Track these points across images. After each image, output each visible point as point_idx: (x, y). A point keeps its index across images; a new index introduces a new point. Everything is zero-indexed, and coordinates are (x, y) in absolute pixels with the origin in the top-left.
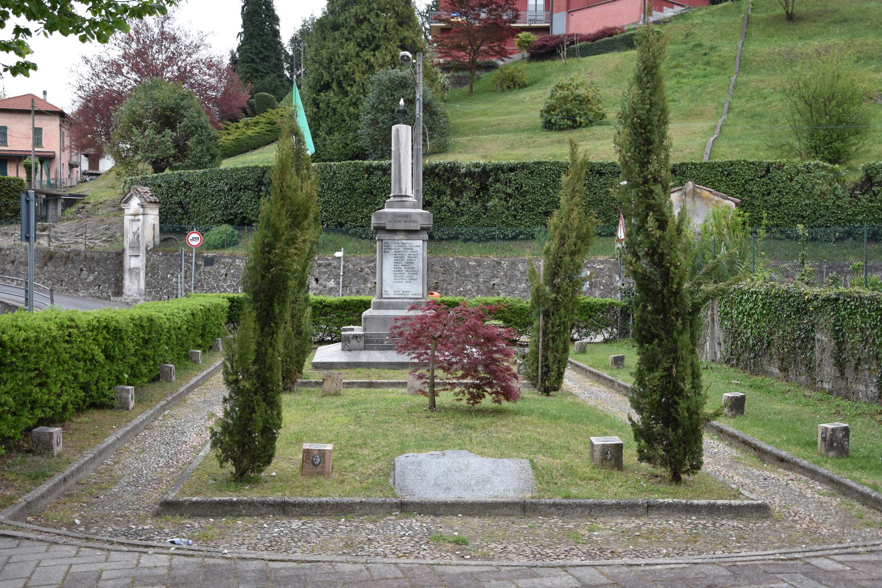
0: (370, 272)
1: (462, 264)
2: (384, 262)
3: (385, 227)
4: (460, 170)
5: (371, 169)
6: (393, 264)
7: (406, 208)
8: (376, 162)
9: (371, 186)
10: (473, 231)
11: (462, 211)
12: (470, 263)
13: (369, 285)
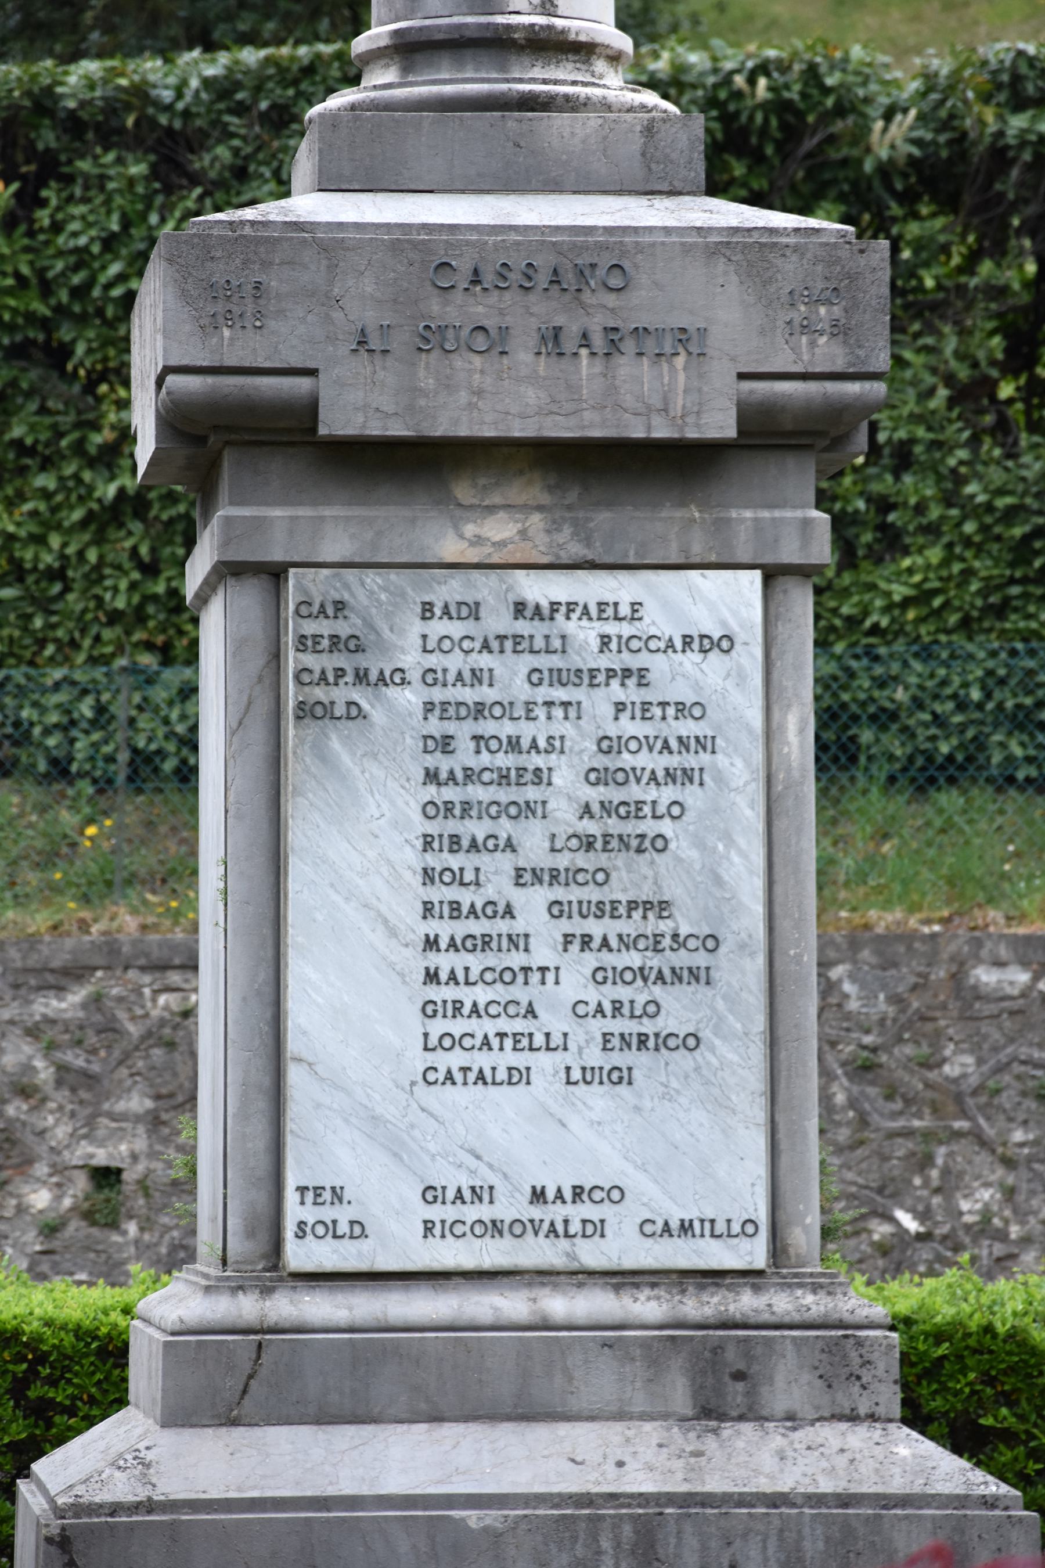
0: (44, 1072)
1: (905, 977)
2: (296, 835)
3: (311, 409)
4: (860, 136)
5: (48, 138)
6: (412, 858)
7: (553, 186)
8: (91, 67)
9: (46, 289)
10: (991, 682)
11: (884, 505)
12: (985, 976)
13: (40, 1199)
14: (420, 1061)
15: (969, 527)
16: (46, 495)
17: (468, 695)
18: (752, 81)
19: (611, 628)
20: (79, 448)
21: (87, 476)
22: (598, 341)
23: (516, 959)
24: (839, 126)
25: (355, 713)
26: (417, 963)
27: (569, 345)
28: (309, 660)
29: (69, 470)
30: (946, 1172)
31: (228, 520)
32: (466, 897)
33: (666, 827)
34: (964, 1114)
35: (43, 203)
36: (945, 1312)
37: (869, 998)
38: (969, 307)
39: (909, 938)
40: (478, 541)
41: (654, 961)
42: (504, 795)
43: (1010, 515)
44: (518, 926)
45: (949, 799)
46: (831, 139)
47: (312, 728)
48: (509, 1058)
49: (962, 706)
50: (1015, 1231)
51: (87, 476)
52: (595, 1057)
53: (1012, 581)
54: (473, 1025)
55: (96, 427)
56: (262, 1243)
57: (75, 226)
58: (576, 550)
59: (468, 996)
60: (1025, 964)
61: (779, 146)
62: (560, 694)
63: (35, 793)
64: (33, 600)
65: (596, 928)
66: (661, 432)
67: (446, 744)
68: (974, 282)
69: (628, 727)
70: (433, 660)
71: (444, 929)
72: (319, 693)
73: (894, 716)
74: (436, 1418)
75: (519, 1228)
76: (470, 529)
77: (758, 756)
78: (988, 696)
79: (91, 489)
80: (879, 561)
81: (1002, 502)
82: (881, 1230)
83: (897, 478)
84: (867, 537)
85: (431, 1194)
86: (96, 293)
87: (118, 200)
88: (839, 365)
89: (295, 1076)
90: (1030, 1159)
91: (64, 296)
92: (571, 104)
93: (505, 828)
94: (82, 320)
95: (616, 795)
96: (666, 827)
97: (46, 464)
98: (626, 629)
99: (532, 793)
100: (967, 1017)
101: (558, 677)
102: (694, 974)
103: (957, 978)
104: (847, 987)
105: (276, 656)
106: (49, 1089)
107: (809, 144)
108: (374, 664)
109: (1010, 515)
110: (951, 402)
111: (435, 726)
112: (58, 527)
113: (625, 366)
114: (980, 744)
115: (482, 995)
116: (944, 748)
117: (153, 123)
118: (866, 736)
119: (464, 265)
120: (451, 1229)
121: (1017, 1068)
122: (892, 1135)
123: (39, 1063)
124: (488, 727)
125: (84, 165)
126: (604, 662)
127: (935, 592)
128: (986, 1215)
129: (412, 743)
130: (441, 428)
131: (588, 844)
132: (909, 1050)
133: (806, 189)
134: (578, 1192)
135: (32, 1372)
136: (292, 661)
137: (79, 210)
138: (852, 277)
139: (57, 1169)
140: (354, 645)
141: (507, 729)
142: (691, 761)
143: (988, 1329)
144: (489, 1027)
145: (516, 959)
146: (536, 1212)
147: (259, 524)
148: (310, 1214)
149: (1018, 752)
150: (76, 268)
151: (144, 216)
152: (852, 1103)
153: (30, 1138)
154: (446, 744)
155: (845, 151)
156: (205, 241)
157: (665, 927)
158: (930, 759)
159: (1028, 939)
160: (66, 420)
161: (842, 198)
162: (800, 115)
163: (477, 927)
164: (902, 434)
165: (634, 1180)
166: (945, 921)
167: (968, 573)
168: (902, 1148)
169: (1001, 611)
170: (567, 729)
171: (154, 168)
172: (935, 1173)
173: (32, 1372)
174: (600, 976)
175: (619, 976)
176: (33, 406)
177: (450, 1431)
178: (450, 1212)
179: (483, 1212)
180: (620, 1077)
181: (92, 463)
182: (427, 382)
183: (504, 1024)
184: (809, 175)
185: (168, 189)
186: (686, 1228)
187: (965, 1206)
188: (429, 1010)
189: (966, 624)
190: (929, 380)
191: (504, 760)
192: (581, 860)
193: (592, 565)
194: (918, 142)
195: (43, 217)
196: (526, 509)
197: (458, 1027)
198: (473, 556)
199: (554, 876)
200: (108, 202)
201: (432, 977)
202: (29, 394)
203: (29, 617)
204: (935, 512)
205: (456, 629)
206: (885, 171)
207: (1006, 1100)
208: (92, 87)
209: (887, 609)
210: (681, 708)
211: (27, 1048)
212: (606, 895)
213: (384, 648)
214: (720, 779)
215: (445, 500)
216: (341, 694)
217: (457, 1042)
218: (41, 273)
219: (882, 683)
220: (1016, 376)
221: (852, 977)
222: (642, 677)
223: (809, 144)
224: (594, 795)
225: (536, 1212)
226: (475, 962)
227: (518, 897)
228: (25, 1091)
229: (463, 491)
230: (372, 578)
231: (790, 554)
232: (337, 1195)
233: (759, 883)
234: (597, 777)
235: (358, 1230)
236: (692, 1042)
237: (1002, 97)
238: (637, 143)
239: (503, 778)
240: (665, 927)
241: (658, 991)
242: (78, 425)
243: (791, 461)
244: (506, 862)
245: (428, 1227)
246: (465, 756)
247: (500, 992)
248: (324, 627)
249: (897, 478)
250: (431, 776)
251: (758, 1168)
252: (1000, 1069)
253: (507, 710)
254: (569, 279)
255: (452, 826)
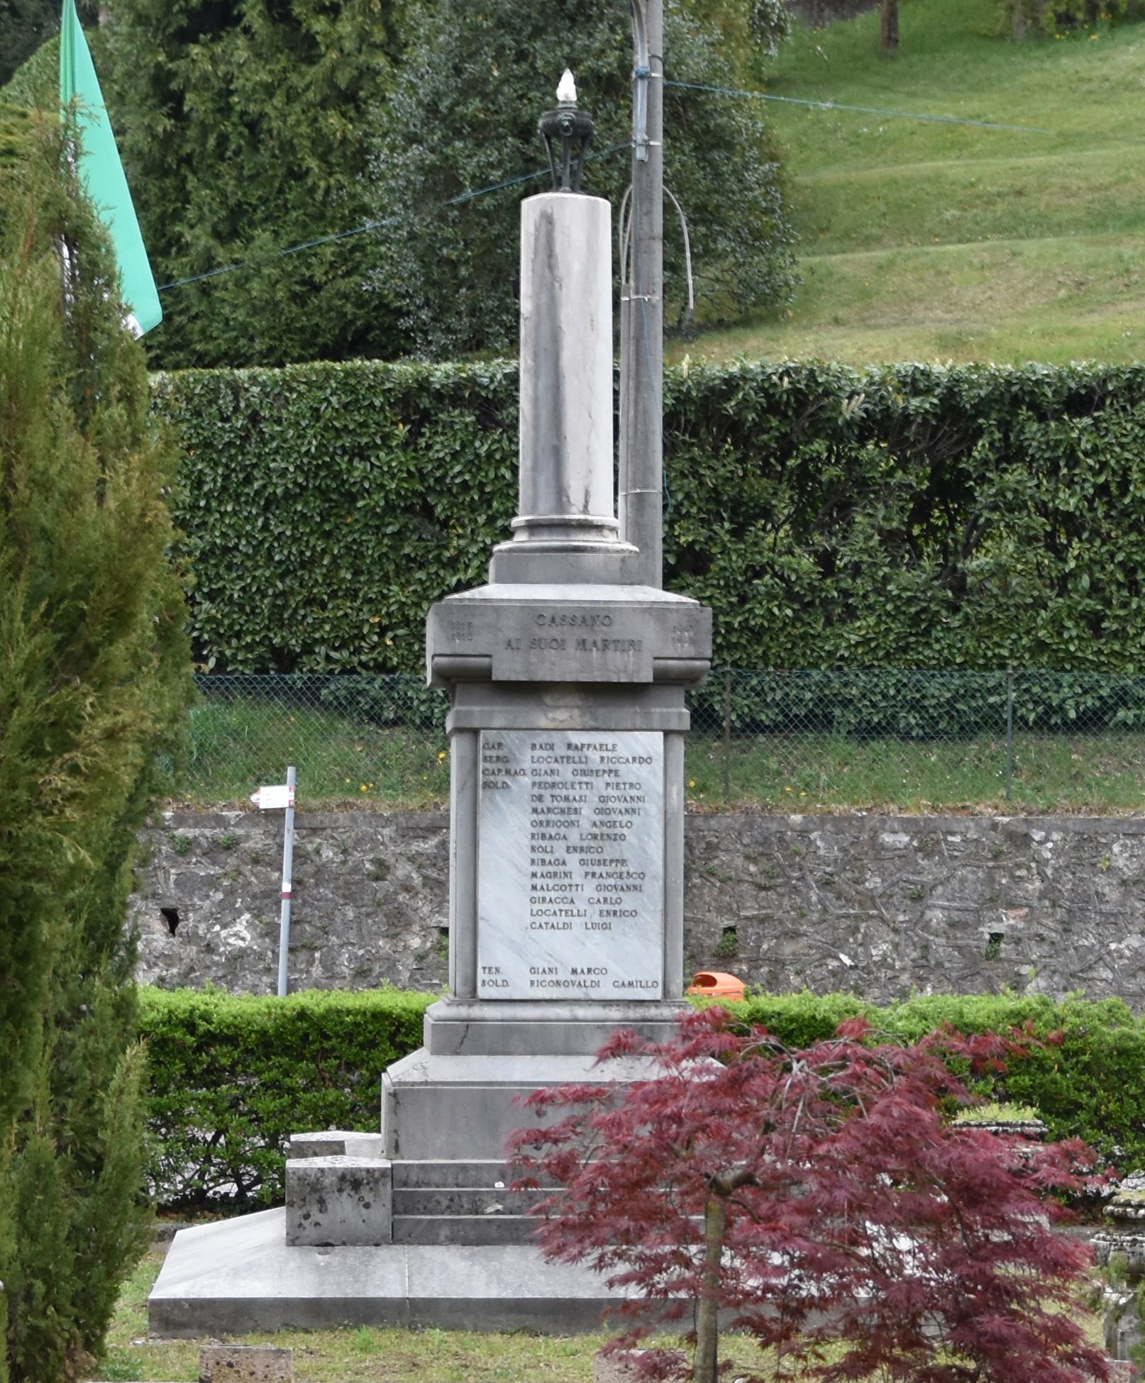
0: (417, 880)
1: (847, 839)
2: (483, 832)
5: (425, 402)
6: (527, 842)
8: (447, 366)
9: (423, 477)
11: (846, 593)
12: (887, 838)
13: (415, 942)
14: (529, 920)
15: (889, 607)
16: (421, 582)
17: (549, 779)
18: (781, 379)
19: (605, 754)
20: (438, 559)
21: (442, 573)
22: (600, 644)
23: (566, 881)
24: (826, 401)
25: (505, 786)
26: (528, 882)
27: (588, 646)
28: (488, 765)
29: (433, 569)
30: (865, 935)
31: (458, 712)
32: (547, 857)
33: (625, 831)
34: (875, 907)
35: (423, 435)
36: (795, 1010)
37: (830, 849)
38: (891, 494)
39: (849, 819)
40: (554, 719)
41: (620, 882)
42: (562, 818)
43: (910, 601)
44: (568, 868)
45: (878, 745)
46: (822, 408)
47: (489, 792)
48: (564, 919)
49: (885, 696)
50: (898, 965)
51: (442, 573)
52: (597, 919)
53: (911, 634)
54: (550, 906)
55: (447, 548)
56: (469, 989)
57: (437, 447)
58: (592, 723)
59: (548, 895)
60: (906, 832)
61: (795, 411)
62: (585, 779)
63: (413, 734)
64: (414, 636)
65: (597, 870)
66: (623, 680)
67: (540, 798)
68: (893, 482)
69: (611, 792)
70: (536, 766)
71: (539, 870)
72: (492, 778)
73: (851, 701)
74: (534, 1053)
75: (566, 984)
76: (551, 715)
77: (661, 803)
78: (898, 691)
79: (443, 579)
80: (844, 623)
81: (906, 595)
82: (833, 964)
83: (854, 579)
84: (839, 610)
85: (533, 970)
86: (448, 481)
87: (460, 434)
88: (692, 654)
89: (481, 924)
90: (906, 930)
91: (431, 481)
92: (593, 550)
93: (563, 831)
94: (440, 494)
95: (605, 818)
96: (625, 831)
97: (422, 566)
98: (610, 754)
99: (573, 817)
100: (878, 859)
101: (584, 773)
102: (635, 887)
103: (874, 838)
104: (819, 843)
105: (475, 764)
106: (419, 888)
107: (811, 410)
108: (513, 768)
109: (910, 601)
110: (881, 543)
111: (536, 791)
112: (427, 598)
113: (610, 654)
114: (894, 716)
115: (553, 895)
116: (876, 719)
117: (479, 395)
118: (837, 712)
119: (548, 615)
120: (541, 983)
121: (902, 884)
122: (839, 917)
123: (414, 875)
124: (556, 792)
125: (442, 416)
126: (601, 767)
127: (872, 639)
128: (884, 957)
129: (527, 797)
130: (540, 676)
131: (595, 837)
132: (849, 875)
133: (809, 432)
134: (589, 970)
135: (398, 1030)
136: (481, 766)
137: (439, 439)
138: (697, 622)
139: (423, 928)
140: (505, 760)
141: (564, 792)
142: (635, 805)
143: (813, 1017)
144: (556, 907)
145: (566, 881)
146: (573, 977)
147: (470, 713)
148: (487, 977)
149: (913, 721)
150: (438, 468)
151: (472, 442)
152: (820, 901)
153: (410, 912)
154: (540, 798)
155: (828, 414)
156: (450, 608)
157: (624, 869)
158: (868, 722)
159: (908, 820)
160: (432, 544)
161: (827, 437)
162: (805, 396)
163: (552, 869)
164: (856, 558)
165: (612, 966)
166: (868, 810)
167: (889, 630)
168: (844, 923)
169: (904, 650)
170: (588, 793)
171: (478, 418)
172: (860, 936)
173: (398, 1030)
174: (599, 888)
175: (606, 888)
176: (415, 537)
177: (539, 1058)
178: (540, 977)
179: (553, 977)
180: (606, 927)
181: (444, 566)
182: (534, 660)
183: (562, 906)
184: (811, 424)
185: (485, 429)
186: (630, 984)
187: (874, 952)
188: (533, 900)
189: (887, 655)
190: (870, 531)
191: (563, 805)
192: (593, 843)
193: (597, 729)
194: (866, 411)
195: (422, 442)
196: (572, 707)
197: (544, 907)
198: (551, 725)
199: (582, 849)
200: (454, 435)
201: (534, 888)
202: (413, 532)
203: (412, 645)
204: (872, 599)
205: (544, 754)
206: (849, 424)
207: (895, 900)
208: (448, 377)
209: (848, 648)
210: (631, 785)
211: (409, 867)
212: (601, 857)
213: (517, 761)
214: (646, 811)
215: (541, 703)
216: (501, 778)
217: (544, 913)
218: (420, 470)
219: (846, 685)
220: (921, 523)
221: (822, 839)
222: (616, 773)
223: (811, 410)
224: (597, 818)
225: (573, 977)
226: (551, 882)
227: (567, 857)
228: (407, 889)
229: (548, 700)
230: (513, 734)
231: (674, 725)
232: (497, 970)
233: (661, 853)
234: (600, 811)
235: (505, 983)
236: (634, 913)
237: (907, 390)
238: (617, 565)
239: (563, 811)
240: (624, 869)
241: (621, 894)
242: (438, 547)
243: (675, 689)
244: (563, 844)
245: (532, 983)
246: (548, 802)
247: (560, 894)
248: (493, 753)
249: (854, 579)
250: (535, 811)
251: (659, 961)
252: (893, 885)
253: (564, 785)
254: (589, 621)
255: (543, 830)
